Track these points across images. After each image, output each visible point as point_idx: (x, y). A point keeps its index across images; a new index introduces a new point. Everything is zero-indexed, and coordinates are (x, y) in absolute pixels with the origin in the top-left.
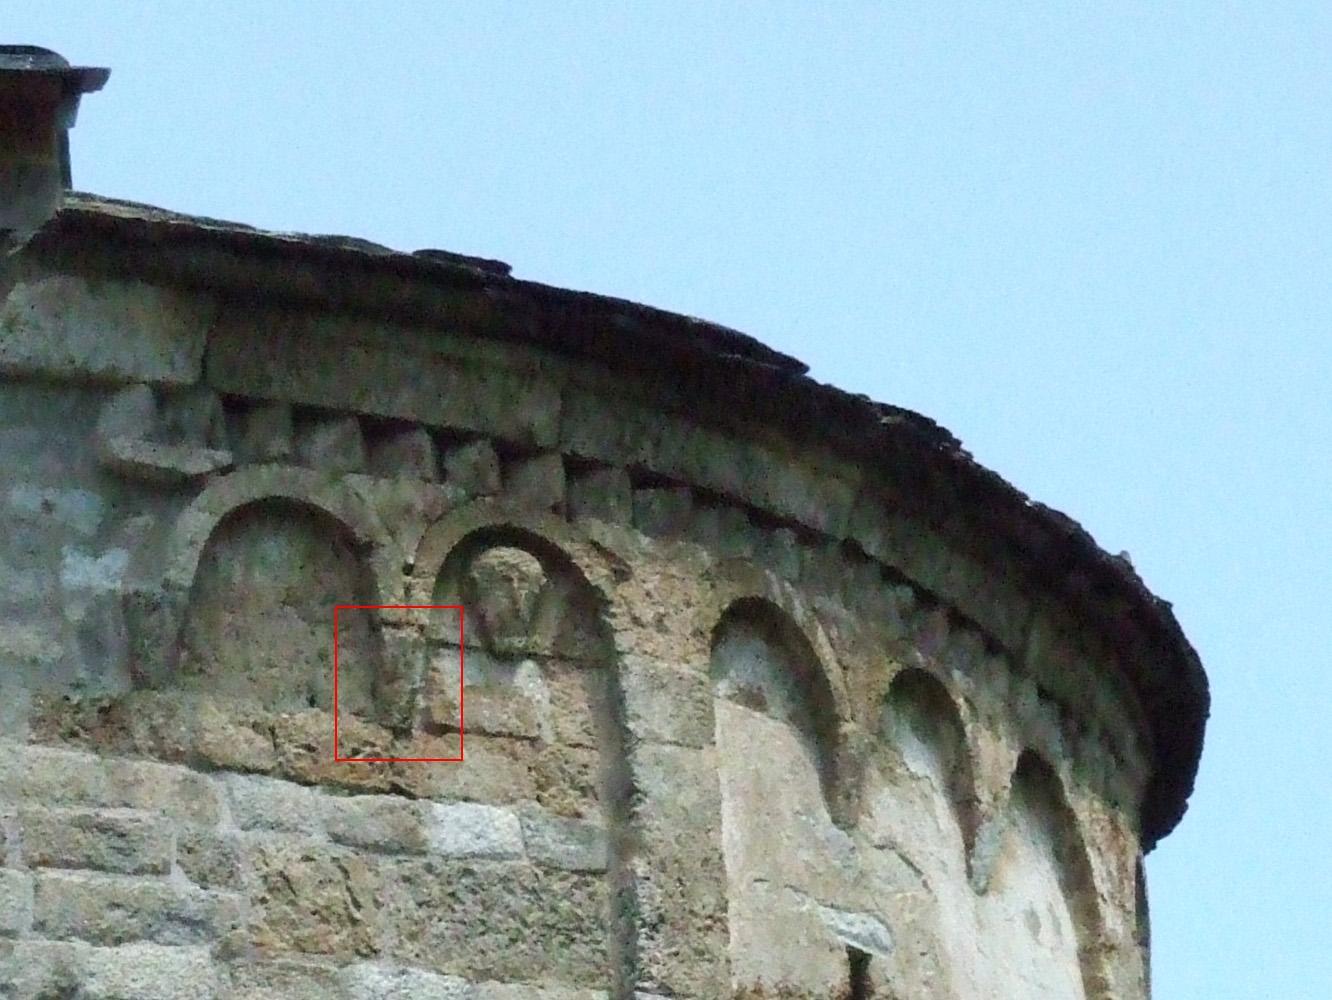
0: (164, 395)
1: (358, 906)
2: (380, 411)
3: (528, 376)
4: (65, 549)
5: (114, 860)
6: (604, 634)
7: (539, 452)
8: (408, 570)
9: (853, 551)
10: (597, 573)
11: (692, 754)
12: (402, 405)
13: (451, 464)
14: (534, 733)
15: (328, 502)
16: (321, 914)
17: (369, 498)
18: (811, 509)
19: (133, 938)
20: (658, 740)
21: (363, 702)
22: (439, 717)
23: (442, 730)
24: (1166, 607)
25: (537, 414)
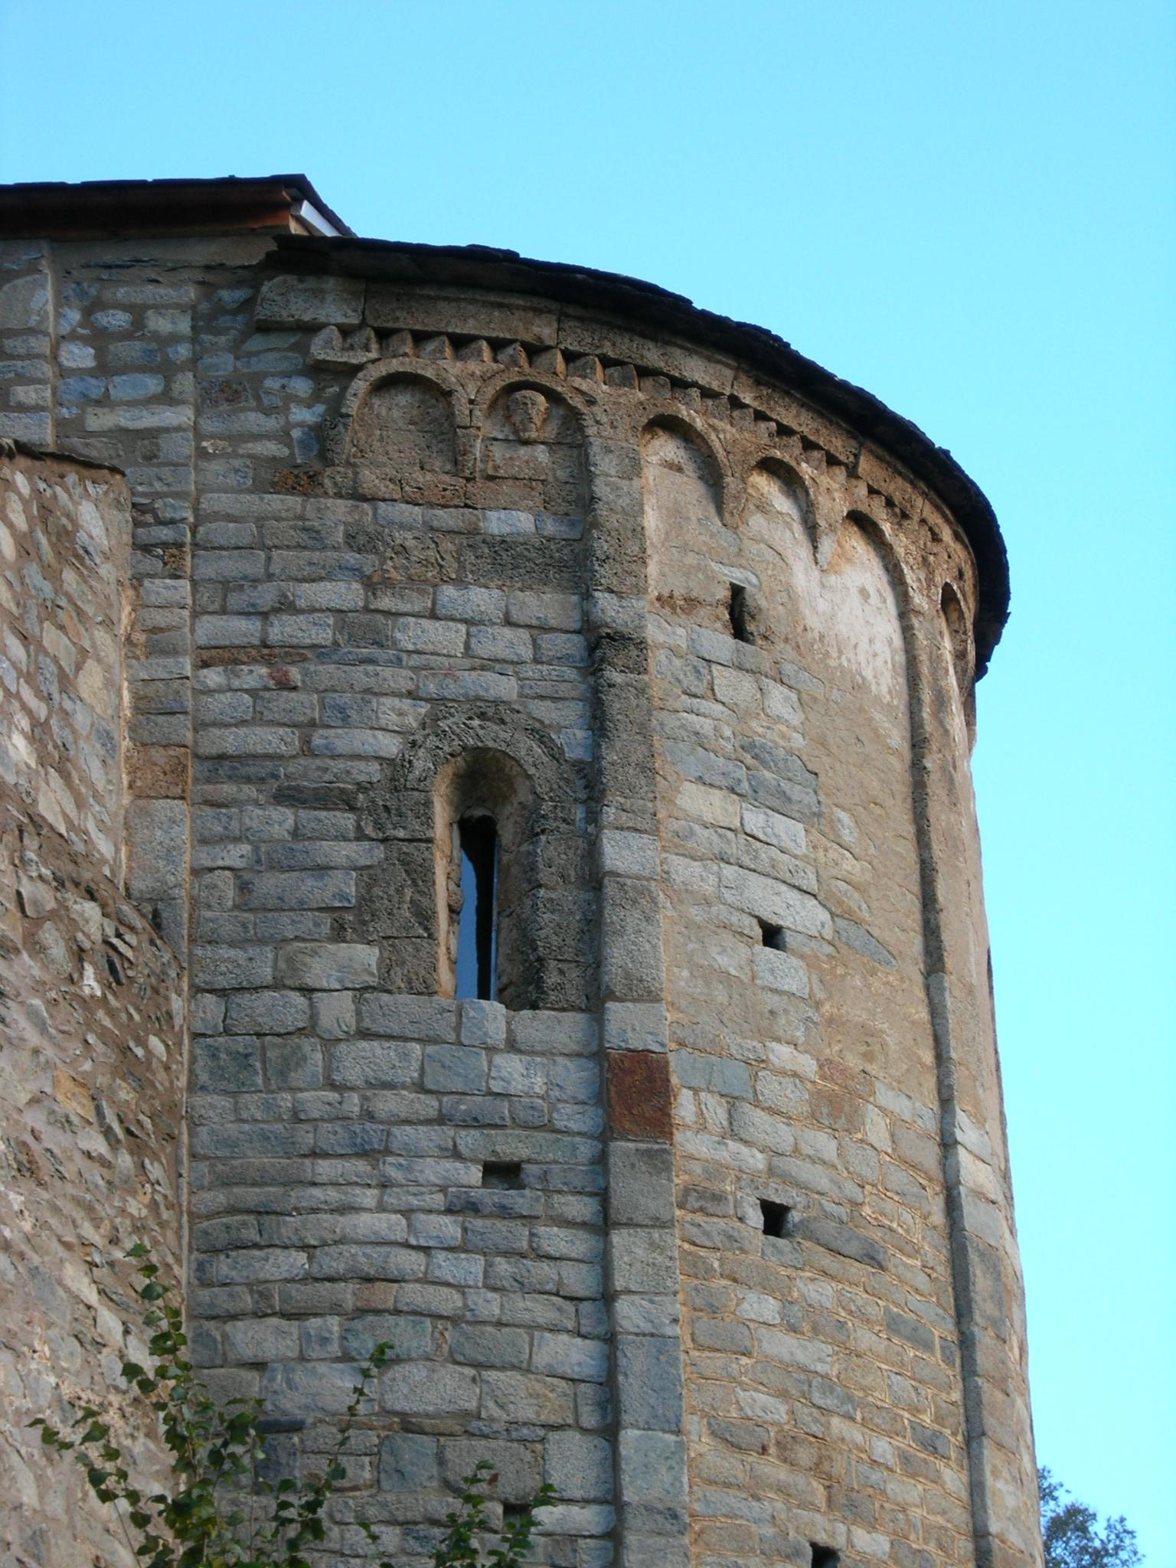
0: (345, 331)
1: (443, 559)
2: (458, 331)
3: (538, 311)
4: (292, 405)
5: (310, 543)
6: (581, 429)
7: (549, 348)
8: (471, 402)
9: (735, 403)
10: (577, 402)
11: (627, 482)
12: (468, 328)
13: (500, 357)
14: (543, 477)
15: (429, 374)
16: (424, 563)
17: (451, 370)
18: (707, 378)
19: (321, 579)
20: (607, 475)
21: (448, 467)
22: (490, 472)
23: (491, 478)
24: (946, 453)
25: (544, 330)
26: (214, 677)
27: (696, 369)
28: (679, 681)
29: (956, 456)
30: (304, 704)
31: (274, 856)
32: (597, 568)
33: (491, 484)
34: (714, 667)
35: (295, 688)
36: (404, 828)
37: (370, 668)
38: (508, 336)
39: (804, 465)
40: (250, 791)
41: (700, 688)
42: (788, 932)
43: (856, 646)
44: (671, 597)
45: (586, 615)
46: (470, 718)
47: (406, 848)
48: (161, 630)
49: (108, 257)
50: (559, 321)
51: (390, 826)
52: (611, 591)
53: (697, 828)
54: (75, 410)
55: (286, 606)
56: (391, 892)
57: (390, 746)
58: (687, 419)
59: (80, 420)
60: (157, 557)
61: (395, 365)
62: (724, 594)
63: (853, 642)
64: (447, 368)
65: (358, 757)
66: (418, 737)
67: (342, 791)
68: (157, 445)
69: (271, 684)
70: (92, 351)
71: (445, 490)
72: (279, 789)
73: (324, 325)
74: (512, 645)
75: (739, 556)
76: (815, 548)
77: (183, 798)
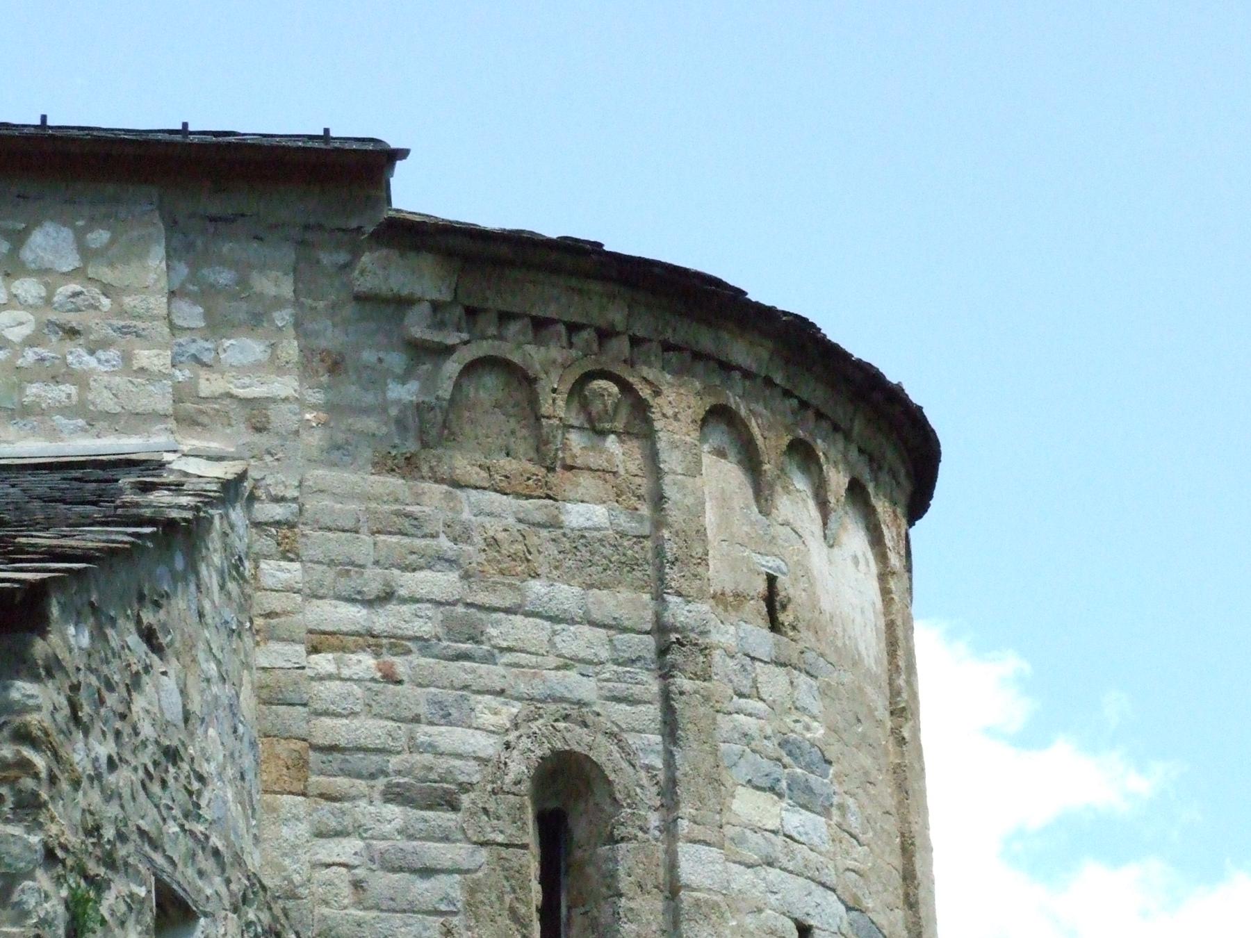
0: (436, 306)
1: (530, 553)
2: (540, 314)
3: (612, 297)
4: (389, 381)
7: (618, 334)
8: (554, 391)
9: (769, 382)
10: (645, 392)
11: (691, 480)
12: (551, 311)
14: (615, 470)
15: (516, 358)
17: (535, 356)
19: (421, 568)
20: (675, 473)
21: (532, 454)
24: (920, 409)
25: (616, 316)
26: (324, 662)
27: (740, 352)
28: (731, 681)
29: (926, 412)
30: (412, 697)
31: (386, 856)
32: (667, 570)
33: (568, 474)
34: (758, 664)
35: (400, 682)
36: (501, 832)
37: (467, 664)
38: (585, 322)
39: (819, 441)
40: (361, 785)
41: (746, 688)
42: (817, 931)
43: (853, 621)
44: (723, 594)
45: (658, 616)
46: (556, 720)
47: (504, 853)
48: (277, 615)
49: (215, 208)
50: (629, 307)
51: (489, 830)
52: (680, 595)
53: (748, 832)
54: (187, 373)
55: (387, 596)
56: (493, 898)
57: (486, 745)
58: (734, 407)
59: (193, 382)
60: (271, 536)
61: (483, 348)
62: (761, 586)
63: (852, 618)
64: (534, 356)
65: (459, 756)
66: (512, 737)
67: (446, 791)
68: (267, 416)
69: (378, 675)
70: (200, 310)
71: (529, 479)
72: (389, 786)
73: (420, 300)
74: (590, 645)
75: (768, 544)
76: (825, 524)
77: (304, 794)
